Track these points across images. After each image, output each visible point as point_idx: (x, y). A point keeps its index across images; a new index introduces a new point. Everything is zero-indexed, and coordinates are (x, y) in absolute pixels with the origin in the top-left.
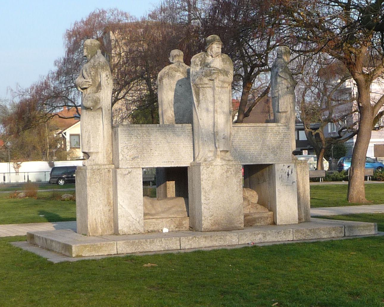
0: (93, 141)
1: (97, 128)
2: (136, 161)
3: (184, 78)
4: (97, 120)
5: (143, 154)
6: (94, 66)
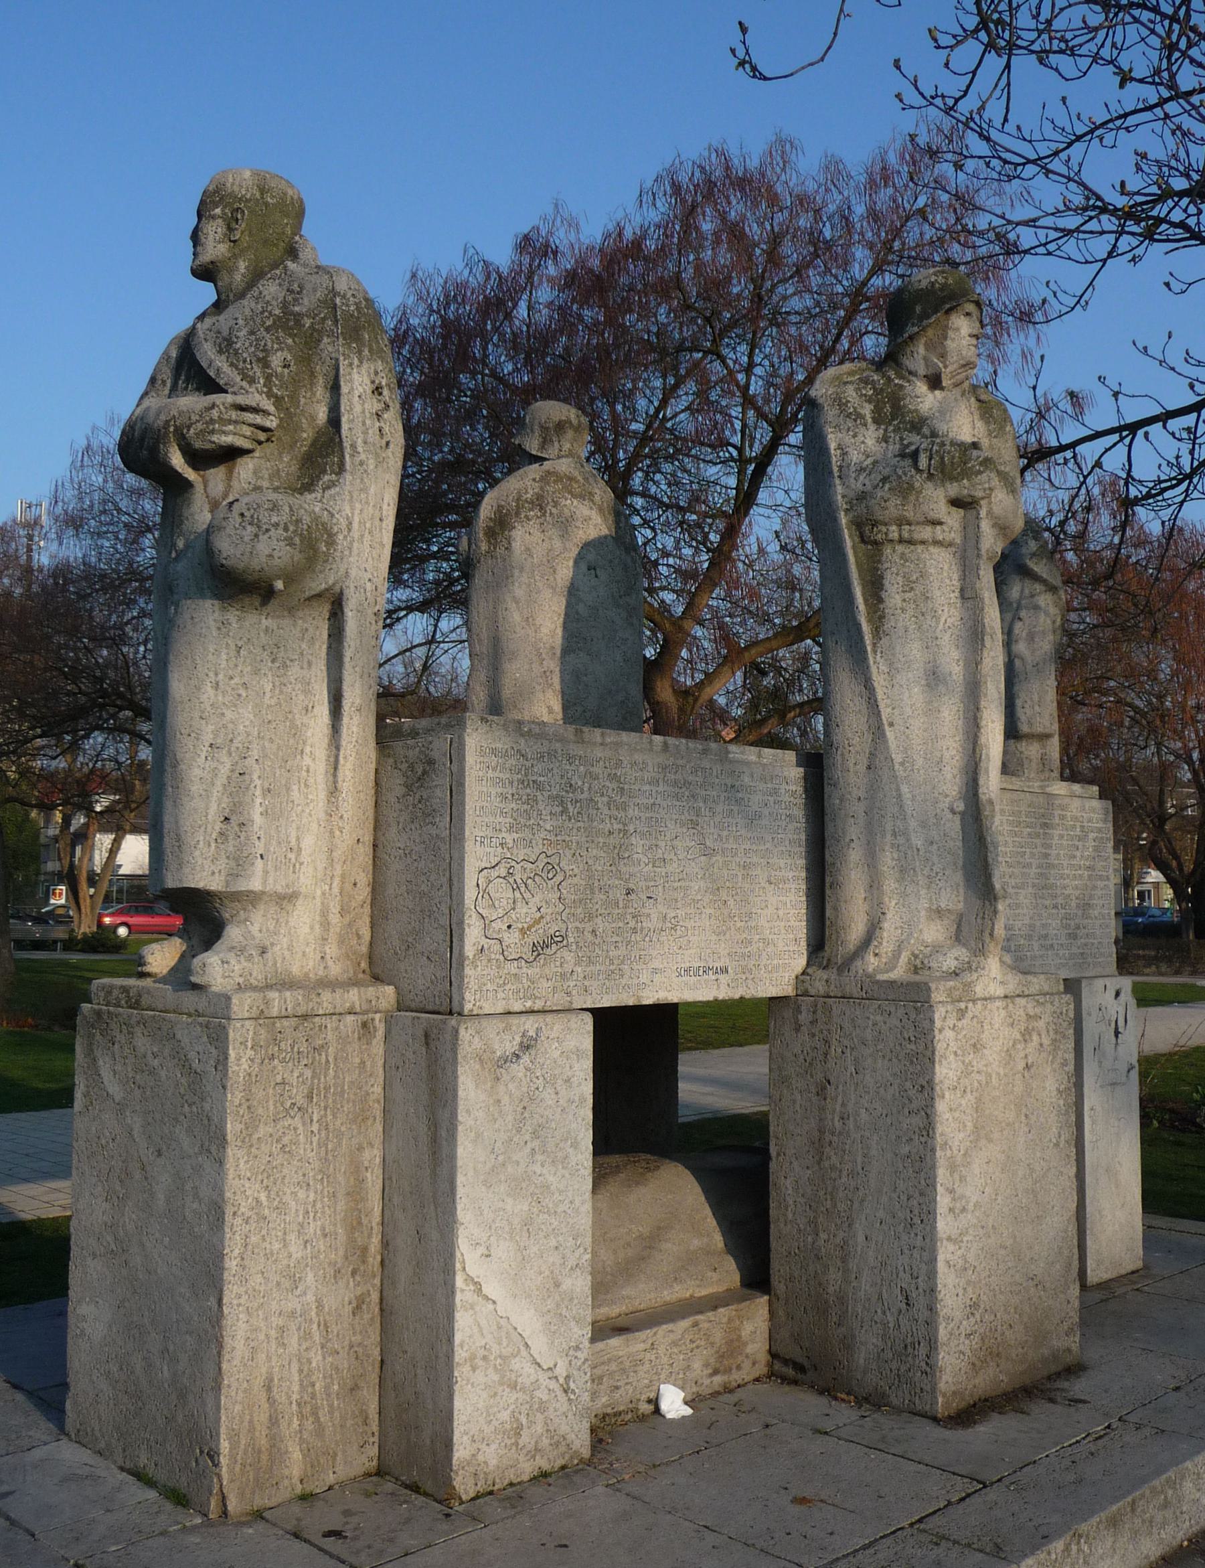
0: (265, 814)
1: (296, 732)
2: (553, 969)
3: (606, 537)
4: (294, 671)
5: (591, 917)
6: (288, 321)
